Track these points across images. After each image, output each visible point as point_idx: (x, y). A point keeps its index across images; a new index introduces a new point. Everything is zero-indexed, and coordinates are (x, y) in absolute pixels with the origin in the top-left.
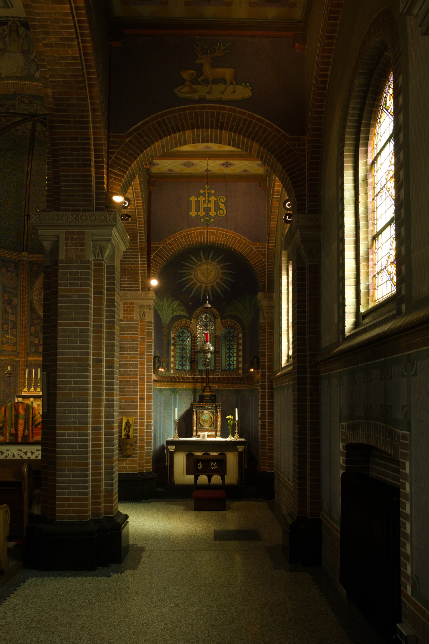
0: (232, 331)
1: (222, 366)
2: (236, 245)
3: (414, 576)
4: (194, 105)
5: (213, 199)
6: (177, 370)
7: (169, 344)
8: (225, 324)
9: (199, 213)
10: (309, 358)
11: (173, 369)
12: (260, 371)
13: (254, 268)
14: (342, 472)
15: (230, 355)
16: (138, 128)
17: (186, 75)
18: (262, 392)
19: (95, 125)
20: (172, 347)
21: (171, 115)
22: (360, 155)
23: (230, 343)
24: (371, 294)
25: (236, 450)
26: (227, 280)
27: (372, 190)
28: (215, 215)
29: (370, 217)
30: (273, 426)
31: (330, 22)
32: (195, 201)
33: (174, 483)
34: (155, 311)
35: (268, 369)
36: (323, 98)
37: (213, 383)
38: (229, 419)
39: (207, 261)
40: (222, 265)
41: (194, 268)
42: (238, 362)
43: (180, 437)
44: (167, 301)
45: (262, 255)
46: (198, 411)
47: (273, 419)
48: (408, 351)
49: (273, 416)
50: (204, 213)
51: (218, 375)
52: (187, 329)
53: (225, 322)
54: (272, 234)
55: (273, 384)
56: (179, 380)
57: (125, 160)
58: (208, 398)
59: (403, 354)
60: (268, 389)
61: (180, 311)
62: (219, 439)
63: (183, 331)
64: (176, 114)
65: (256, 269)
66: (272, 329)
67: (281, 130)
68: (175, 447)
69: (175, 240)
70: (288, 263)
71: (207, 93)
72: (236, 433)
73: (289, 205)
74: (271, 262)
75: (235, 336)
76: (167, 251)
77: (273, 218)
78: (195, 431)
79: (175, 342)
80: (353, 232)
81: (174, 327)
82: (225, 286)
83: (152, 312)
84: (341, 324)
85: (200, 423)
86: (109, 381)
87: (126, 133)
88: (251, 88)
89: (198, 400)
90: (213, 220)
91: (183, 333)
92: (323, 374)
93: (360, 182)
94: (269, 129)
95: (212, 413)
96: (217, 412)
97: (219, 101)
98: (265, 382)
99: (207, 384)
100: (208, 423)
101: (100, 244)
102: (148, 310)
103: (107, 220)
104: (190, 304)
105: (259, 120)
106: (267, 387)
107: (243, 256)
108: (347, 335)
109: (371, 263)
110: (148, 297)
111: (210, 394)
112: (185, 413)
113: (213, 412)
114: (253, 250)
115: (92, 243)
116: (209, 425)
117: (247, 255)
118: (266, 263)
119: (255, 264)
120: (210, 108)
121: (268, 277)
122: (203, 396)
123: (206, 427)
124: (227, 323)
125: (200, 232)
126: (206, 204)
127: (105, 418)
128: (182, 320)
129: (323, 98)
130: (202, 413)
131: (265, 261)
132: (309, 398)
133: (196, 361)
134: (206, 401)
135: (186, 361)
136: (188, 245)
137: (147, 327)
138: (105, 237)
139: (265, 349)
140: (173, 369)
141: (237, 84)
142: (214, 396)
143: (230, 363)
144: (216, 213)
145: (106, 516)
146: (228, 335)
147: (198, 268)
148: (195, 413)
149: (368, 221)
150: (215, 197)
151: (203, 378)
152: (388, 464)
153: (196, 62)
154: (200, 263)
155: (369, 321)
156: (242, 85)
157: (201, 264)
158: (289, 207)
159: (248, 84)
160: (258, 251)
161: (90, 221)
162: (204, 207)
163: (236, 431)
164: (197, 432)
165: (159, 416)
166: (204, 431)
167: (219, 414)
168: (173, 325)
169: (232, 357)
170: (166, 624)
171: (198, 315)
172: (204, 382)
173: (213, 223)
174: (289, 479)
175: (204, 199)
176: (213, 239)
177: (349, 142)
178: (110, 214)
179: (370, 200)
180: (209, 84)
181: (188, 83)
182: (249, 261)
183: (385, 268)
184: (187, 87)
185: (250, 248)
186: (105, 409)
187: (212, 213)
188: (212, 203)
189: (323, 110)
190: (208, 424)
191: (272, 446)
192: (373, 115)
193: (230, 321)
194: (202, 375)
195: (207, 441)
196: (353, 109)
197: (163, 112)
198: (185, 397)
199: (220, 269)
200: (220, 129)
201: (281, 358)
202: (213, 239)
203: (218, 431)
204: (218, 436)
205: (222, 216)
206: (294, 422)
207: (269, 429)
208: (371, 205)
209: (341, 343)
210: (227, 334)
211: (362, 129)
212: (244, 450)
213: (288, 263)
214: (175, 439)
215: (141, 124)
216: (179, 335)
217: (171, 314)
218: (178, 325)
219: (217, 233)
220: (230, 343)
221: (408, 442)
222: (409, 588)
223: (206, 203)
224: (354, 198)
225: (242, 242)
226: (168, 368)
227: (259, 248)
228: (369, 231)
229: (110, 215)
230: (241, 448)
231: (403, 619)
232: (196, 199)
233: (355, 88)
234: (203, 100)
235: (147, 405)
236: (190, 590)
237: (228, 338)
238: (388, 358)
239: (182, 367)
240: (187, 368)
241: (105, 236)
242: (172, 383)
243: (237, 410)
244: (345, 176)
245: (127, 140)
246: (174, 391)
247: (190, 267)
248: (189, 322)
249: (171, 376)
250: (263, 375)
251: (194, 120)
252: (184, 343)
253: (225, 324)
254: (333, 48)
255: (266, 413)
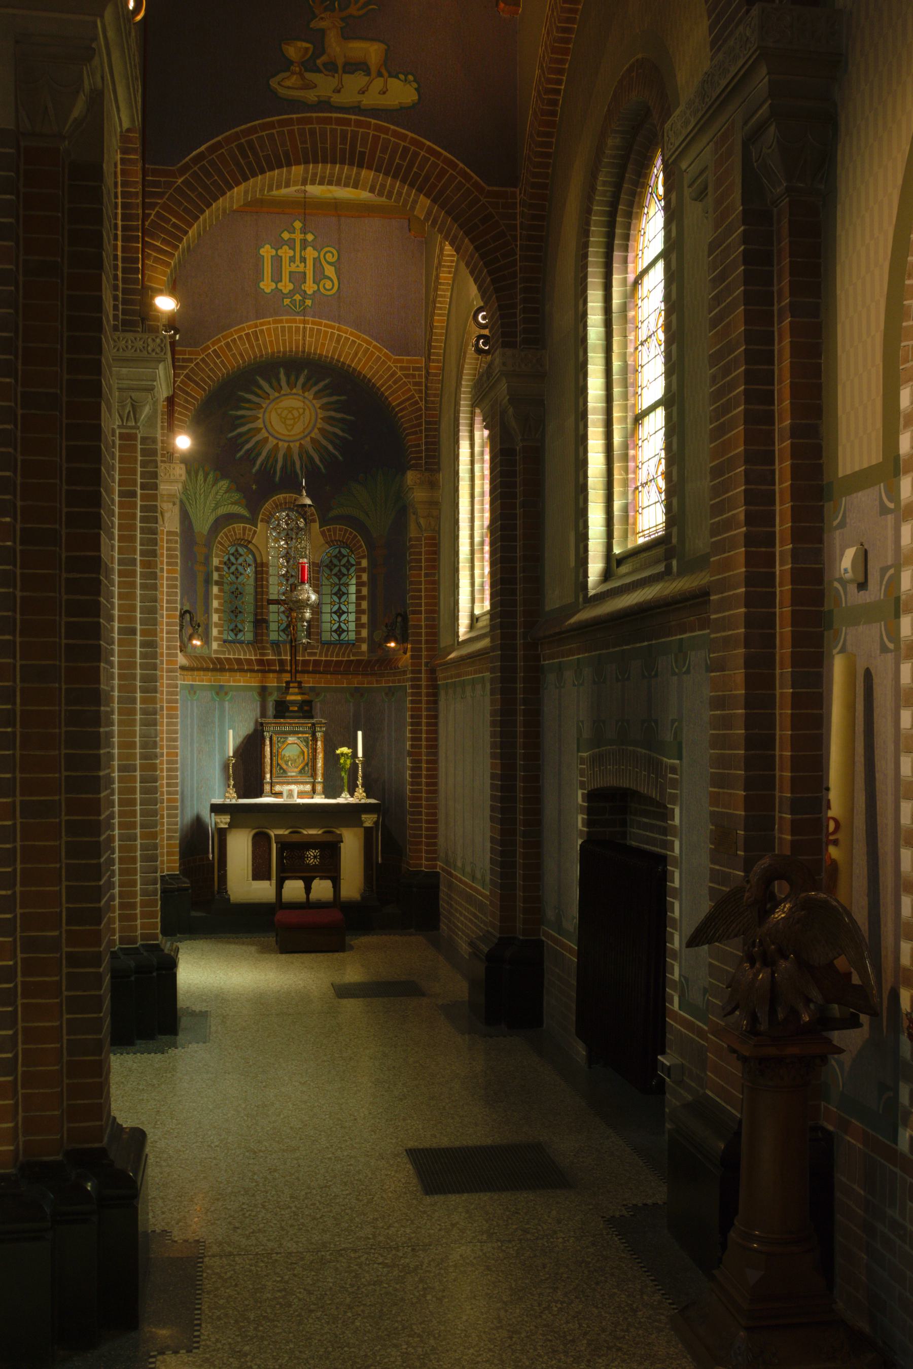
0: (344, 551)
1: (323, 634)
2: (360, 360)
3: (683, 979)
4: (308, 115)
5: (310, 253)
6: (225, 641)
7: (208, 581)
8: (330, 535)
9: (280, 285)
10: (522, 630)
11: (216, 639)
12: (409, 646)
13: (397, 413)
14: (580, 842)
15: (340, 608)
16: (201, 156)
17: (294, 50)
18: (413, 694)
19: (127, 157)
20: (215, 590)
21: (264, 133)
22: (615, 265)
23: (340, 579)
24: (631, 521)
25: (359, 823)
26: (335, 434)
27: (633, 331)
28: (314, 291)
29: (630, 381)
30: (436, 769)
31: (565, 5)
32: (272, 256)
33: (229, 899)
34: (181, 501)
35: (427, 642)
36: (551, 130)
37: (303, 672)
38: (342, 754)
39: (291, 389)
40: (325, 400)
41: (264, 406)
42: (359, 626)
43: (239, 797)
44: (205, 480)
45: (415, 384)
46: (275, 738)
47: (436, 754)
48: (680, 635)
49: (436, 747)
50: (291, 286)
51: (314, 654)
52: (246, 547)
53: (329, 530)
54: (437, 341)
55: (436, 678)
56: (232, 667)
57: (177, 221)
58: (296, 709)
59: (674, 638)
60: (427, 687)
61: (232, 504)
62: (319, 800)
63: (237, 550)
64: (274, 131)
65: (402, 417)
66: (435, 553)
67: (472, 174)
68: (231, 819)
69: (228, 345)
70: (473, 413)
71: (334, 92)
72: (358, 787)
73: (484, 318)
74: (433, 402)
75: (352, 565)
76: (211, 370)
77: (440, 308)
78: (268, 783)
79: (221, 576)
80: (601, 405)
81: (220, 543)
82: (330, 448)
83: (177, 510)
84: (581, 571)
85: (278, 764)
86: (147, 674)
87: (179, 165)
88: (415, 85)
89: (271, 710)
90: (310, 301)
91: (238, 556)
92: (547, 662)
93: (614, 315)
94: (451, 171)
95: (305, 741)
96: (315, 740)
97: (357, 109)
98: (420, 672)
99: (293, 676)
100: (297, 765)
101: (133, 395)
102: (170, 505)
103: (149, 348)
104: (254, 487)
105: (431, 151)
106: (424, 683)
107: (374, 385)
108: (591, 592)
109: (631, 464)
110: (172, 477)
111: (299, 698)
112: (242, 742)
113: (306, 741)
114: (394, 373)
115: (117, 394)
116: (299, 769)
117: (382, 385)
118: (422, 404)
119: (399, 405)
120: (340, 121)
121: (426, 436)
122: (284, 702)
123: (293, 773)
124: (335, 534)
125: (283, 328)
126: (296, 265)
127: (142, 747)
128: (235, 525)
129: (551, 130)
130: (284, 742)
131: (421, 398)
132: (523, 707)
133: (266, 621)
134: (292, 714)
135: (243, 622)
136: (256, 357)
137: (167, 543)
138: (144, 383)
139: (420, 598)
140: (216, 639)
141: (391, 76)
142: (309, 703)
143: (340, 627)
144: (316, 288)
145: (145, 942)
146: (336, 561)
147: (271, 406)
148: (268, 742)
149: (626, 387)
150: (315, 249)
151: (282, 662)
152: (654, 822)
153: (313, 25)
154: (277, 394)
155: (627, 571)
156: (399, 79)
157: (278, 398)
158: (484, 322)
159: (411, 77)
160: (406, 376)
161: (115, 350)
162: (290, 272)
163: (360, 782)
164: (272, 784)
165: (189, 749)
166: (289, 783)
167: (319, 743)
168: (216, 538)
169: (344, 612)
170: (294, 1105)
171: (270, 513)
172: (286, 671)
173: (311, 308)
174: (473, 878)
175: (291, 253)
176: (310, 346)
177: (596, 239)
178: (154, 337)
179: (631, 349)
180: (337, 72)
181: (297, 69)
182: (387, 398)
183: (654, 479)
184: (295, 76)
185: (389, 368)
186: (140, 730)
187: (310, 287)
188: (308, 262)
189: (551, 151)
190: (297, 767)
191: (435, 814)
192: (637, 199)
193: (340, 530)
194: (280, 654)
195: (298, 805)
196: (604, 183)
197: (249, 125)
198: (244, 704)
199: (314, 398)
200: (357, 166)
201: (458, 619)
202: (310, 346)
203: (319, 782)
204: (319, 794)
205: (329, 293)
206: (493, 756)
207: (427, 777)
208: (632, 359)
209: (581, 607)
210: (333, 559)
211: (619, 219)
212: (376, 823)
213: (473, 413)
214: (228, 801)
215: (207, 149)
216: (229, 559)
217: (213, 510)
218: (226, 536)
219: (319, 331)
220: (340, 579)
221: (677, 777)
222: (676, 1000)
223: (294, 262)
224: (604, 342)
225: (373, 353)
226: (206, 639)
227: (408, 369)
228: (629, 405)
229: (153, 340)
230: (369, 820)
231: (668, 1051)
232: (274, 252)
233: (608, 152)
234: (324, 105)
235: (168, 724)
236: (318, 1065)
237: (337, 569)
238: (654, 642)
239: (236, 635)
240: (249, 636)
241: (143, 380)
242: (215, 673)
243: (360, 733)
244: (589, 300)
245: (180, 181)
246: (220, 691)
247: (255, 403)
248: (250, 530)
249: (213, 656)
250: (416, 657)
251: (309, 146)
252: (239, 580)
253: (330, 535)
254: (570, 46)
255: (421, 741)
